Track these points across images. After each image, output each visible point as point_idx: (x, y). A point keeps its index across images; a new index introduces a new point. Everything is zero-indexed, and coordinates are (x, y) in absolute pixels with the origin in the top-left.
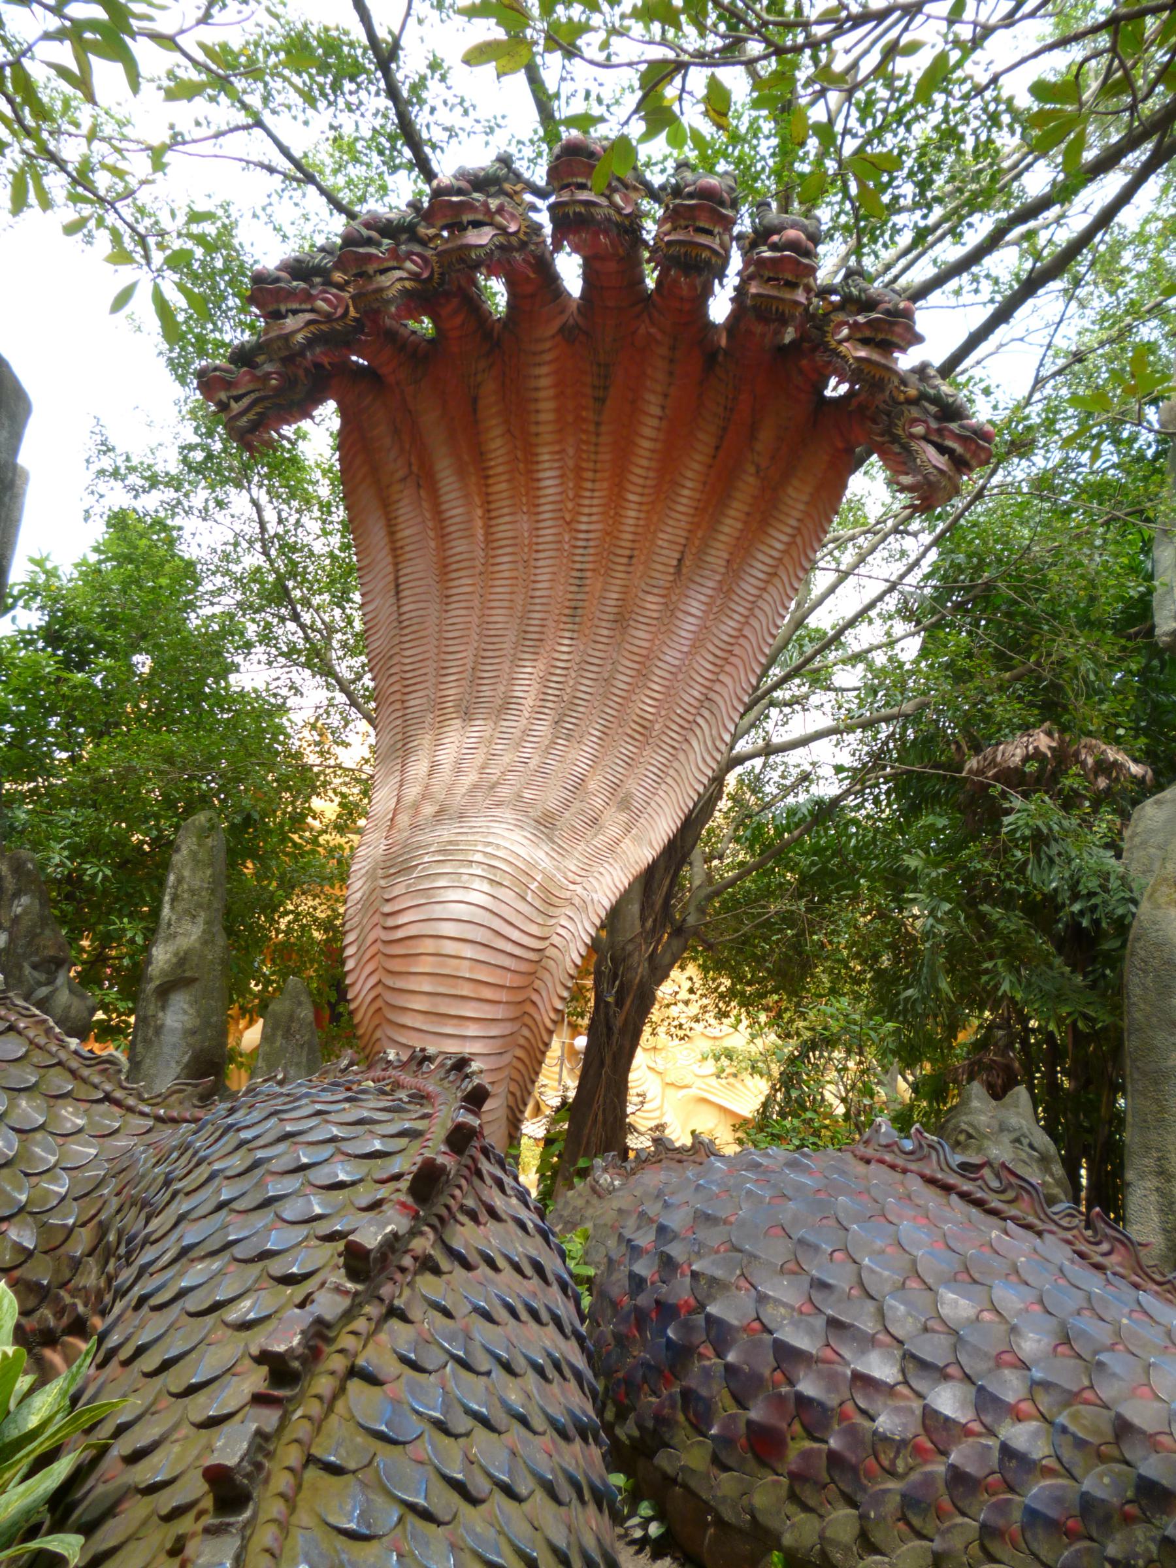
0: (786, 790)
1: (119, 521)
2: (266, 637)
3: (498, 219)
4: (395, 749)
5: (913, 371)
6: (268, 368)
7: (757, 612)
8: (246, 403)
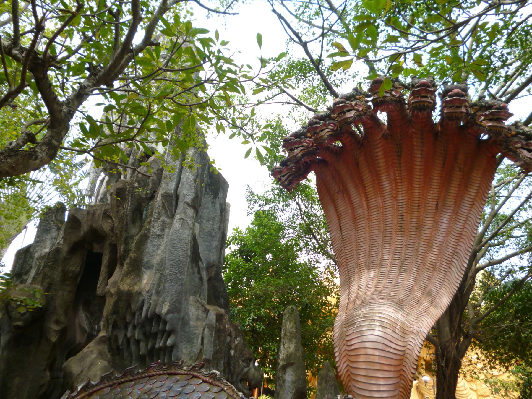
0: (504, 277)
1: (258, 215)
2: (307, 245)
3: (356, 107)
4: (347, 282)
5: (513, 125)
6: (291, 165)
7: (469, 218)
8: (288, 177)
